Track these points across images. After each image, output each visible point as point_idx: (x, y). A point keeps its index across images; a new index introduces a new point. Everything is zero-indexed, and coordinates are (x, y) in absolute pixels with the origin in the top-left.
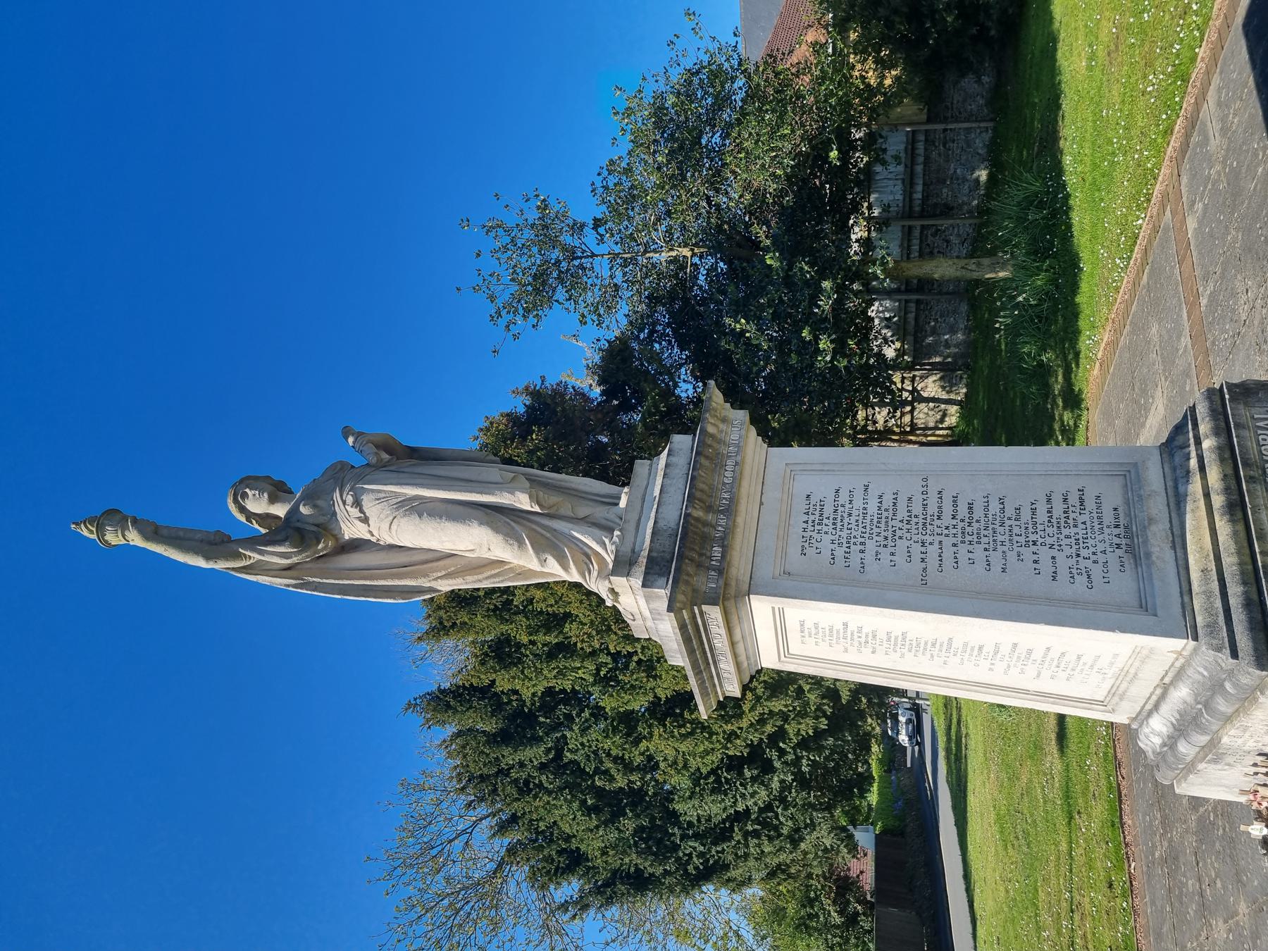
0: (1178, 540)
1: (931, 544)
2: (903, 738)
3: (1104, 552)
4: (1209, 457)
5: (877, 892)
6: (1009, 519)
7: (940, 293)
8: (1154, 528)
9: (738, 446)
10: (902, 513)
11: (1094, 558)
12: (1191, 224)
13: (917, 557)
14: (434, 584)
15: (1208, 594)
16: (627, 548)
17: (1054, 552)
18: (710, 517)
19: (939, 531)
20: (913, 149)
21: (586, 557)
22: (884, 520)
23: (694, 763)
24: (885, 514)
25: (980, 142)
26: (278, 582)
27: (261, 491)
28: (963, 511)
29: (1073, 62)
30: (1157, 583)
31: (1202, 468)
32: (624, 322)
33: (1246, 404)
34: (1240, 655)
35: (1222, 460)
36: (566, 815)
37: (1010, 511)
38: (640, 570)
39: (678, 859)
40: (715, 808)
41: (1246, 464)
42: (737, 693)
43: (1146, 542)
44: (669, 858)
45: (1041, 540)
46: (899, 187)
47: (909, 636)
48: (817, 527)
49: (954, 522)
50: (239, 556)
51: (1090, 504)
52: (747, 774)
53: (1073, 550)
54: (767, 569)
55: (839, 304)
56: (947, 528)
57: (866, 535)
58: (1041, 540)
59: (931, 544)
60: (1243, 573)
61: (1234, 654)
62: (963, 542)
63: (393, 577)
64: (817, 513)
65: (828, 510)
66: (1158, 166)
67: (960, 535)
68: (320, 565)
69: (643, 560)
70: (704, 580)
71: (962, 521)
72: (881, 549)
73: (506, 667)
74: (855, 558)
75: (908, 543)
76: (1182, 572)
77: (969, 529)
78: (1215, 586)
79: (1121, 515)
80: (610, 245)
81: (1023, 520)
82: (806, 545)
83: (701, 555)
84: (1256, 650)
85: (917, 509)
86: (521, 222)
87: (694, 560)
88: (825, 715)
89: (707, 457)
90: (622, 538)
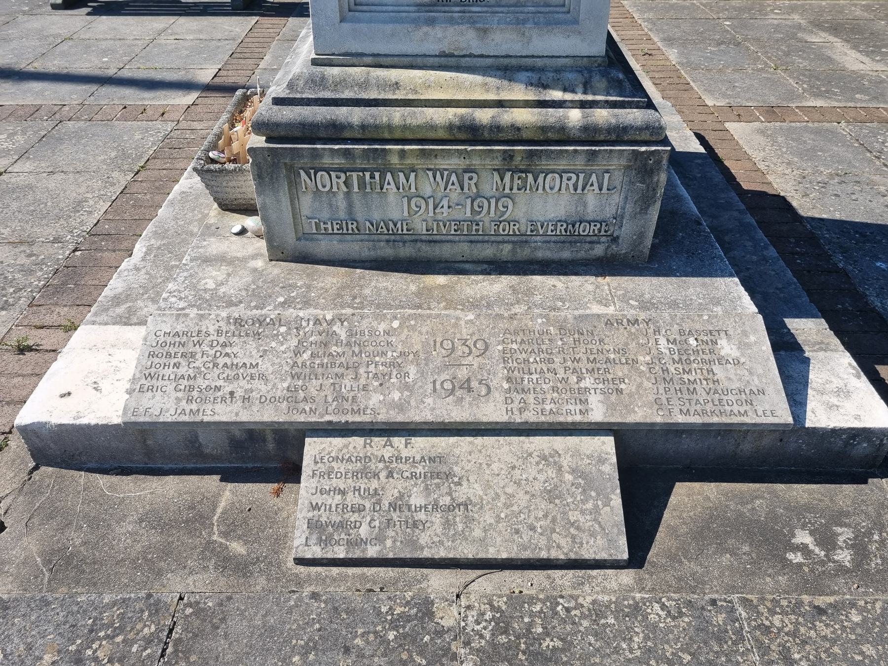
0: (452, 61)
4: (552, 115)
15: (365, 85)
30: (389, 28)
33: (628, 168)
34: (276, 107)
35: (544, 129)
41: (531, 154)
43: (452, 22)
60: (377, 127)
61: (278, 101)
76: (406, 60)
78: (373, 95)
84: (277, 125)
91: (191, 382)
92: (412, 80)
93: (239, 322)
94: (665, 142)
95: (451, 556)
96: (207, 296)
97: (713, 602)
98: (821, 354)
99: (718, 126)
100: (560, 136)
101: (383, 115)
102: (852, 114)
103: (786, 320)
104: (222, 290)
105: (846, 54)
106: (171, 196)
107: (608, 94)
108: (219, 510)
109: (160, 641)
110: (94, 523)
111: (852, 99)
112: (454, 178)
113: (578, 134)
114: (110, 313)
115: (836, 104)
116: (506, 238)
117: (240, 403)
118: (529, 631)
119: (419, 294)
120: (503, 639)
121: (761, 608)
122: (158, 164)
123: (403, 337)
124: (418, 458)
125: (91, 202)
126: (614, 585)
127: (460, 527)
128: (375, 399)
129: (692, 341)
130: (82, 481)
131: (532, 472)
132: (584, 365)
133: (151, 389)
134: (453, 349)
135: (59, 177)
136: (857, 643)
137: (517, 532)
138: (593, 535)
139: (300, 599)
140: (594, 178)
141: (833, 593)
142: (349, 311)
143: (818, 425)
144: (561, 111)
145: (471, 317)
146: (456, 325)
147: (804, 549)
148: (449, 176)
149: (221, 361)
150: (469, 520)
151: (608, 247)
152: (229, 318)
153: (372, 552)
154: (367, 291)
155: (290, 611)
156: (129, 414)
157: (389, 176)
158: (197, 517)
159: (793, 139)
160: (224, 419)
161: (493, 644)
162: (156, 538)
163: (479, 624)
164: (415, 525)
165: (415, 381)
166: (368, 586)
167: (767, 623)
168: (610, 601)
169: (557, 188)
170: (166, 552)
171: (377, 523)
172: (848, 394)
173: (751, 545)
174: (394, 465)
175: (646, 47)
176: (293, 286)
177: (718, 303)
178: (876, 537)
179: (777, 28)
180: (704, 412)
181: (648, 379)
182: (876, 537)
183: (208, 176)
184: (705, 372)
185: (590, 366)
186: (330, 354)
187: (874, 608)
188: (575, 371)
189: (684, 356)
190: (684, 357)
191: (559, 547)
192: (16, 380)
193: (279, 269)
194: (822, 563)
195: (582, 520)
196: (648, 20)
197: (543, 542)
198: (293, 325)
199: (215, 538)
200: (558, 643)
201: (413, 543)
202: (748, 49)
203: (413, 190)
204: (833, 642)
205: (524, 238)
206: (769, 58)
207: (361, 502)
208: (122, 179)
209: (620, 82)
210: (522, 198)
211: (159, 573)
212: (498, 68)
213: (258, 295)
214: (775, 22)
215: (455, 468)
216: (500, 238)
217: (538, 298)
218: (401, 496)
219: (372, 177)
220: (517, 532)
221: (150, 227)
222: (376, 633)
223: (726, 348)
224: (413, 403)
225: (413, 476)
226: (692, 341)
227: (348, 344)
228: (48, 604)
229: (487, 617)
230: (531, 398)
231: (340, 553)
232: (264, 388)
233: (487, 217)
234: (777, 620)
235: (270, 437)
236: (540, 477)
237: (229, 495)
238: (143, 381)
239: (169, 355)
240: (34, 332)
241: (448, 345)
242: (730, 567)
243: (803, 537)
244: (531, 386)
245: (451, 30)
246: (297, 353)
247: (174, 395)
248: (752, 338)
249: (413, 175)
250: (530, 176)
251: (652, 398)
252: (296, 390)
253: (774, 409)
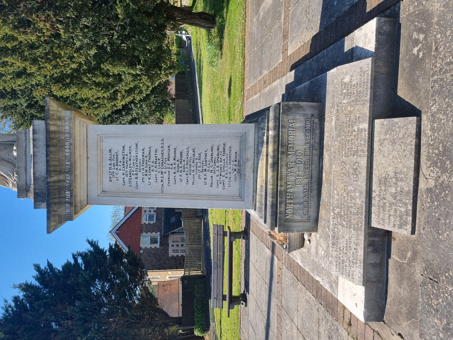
0: (255, 169)
1: (165, 173)
3: (230, 173)
4: (271, 140)
5: (176, 95)
6: (196, 159)
8: (248, 163)
9: (69, 133)
10: (153, 159)
11: (226, 176)
13: (159, 179)
15: (261, 196)
16: (23, 182)
17: (212, 174)
18: (61, 177)
19: (168, 166)
22: (145, 162)
24: (146, 159)
28: (178, 154)
30: (246, 187)
33: (287, 115)
35: (274, 142)
37: (197, 156)
38: (31, 196)
43: (245, 169)
45: (208, 169)
48: (116, 167)
49: (174, 162)
51: (227, 151)
53: (219, 173)
54: (95, 191)
56: (172, 165)
57: (138, 170)
58: (208, 169)
59: (165, 173)
61: (265, 222)
62: (178, 171)
64: (115, 159)
67: (177, 168)
70: (64, 208)
71: (178, 161)
72: (145, 177)
74: (134, 181)
75: (155, 173)
76: (255, 183)
77: (180, 165)
79: (238, 155)
81: (202, 159)
82: (111, 176)
83: (60, 198)
84: (272, 223)
85: (159, 156)
89: (53, 146)
90: (19, 177)
91: (351, 262)
93: (333, 244)
94: (279, 104)
95: (413, 180)
96: (326, 254)
97: (432, 87)
98: (355, 41)
99: (289, 58)
100: (277, 137)
101: (269, 191)
102: (287, 4)
103: (345, 51)
104: (325, 249)
105: (267, 2)
106: (302, 266)
107: (265, 122)
108: (398, 260)
109: (433, 283)
110: (400, 303)
111: (282, 3)
112: (289, 170)
113: (276, 132)
114: (335, 289)
115: (283, 10)
116: (311, 152)
117: (358, 247)
118: (437, 155)
119: (327, 183)
120: (439, 164)
121: (435, 70)
122: (295, 272)
123: (339, 190)
124: (379, 188)
125: (307, 297)
126: (426, 122)
127: (403, 176)
128: (358, 201)
129: (344, 91)
130: (388, 306)
131: (385, 149)
132: (350, 129)
133: (353, 275)
134: (344, 173)
135: (299, 308)
136: (446, 37)
137: (405, 156)
138: (407, 129)
139: (424, 234)
140: (290, 125)
141: (432, 42)
142: (331, 207)
143: (374, 47)
144: (269, 137)
145: (334, 166)
146: (337, 172)
147: (419, 51)
148: (288, 171)
149: (345, 251)
150: (401, 173)
151: (315, 117)
152: (332, 247)
153: (410, 207)
154: (326, 200)
155: (427, 238)
156: (360, 283)
157: (288, 190)
158: (400, 267)
159: (294, 30)
160: (363, 252)
161: (440, 168)
162: (405, 282)
163: (434, 172)
164: (402, 191)
165: (353, 187)
166: (422, 210)
167: (439, 69)
168: (430, 124)
169: (294, 137)
170: (409, 279)
171: (400, 205)
172: (366, 34)
173: (417, 70)
174: (381, 197)
175: (262, 82)
176: (324, 225)
177: (334, 81)
178: (416, 24)
179: (258, 29)
180: (367, 88)
181: (356, 107)
182: (416, 24)
183: (291, 249)
184: (354, 87)
185: (351, 127)
186: (344, 215)
187: (437, 29)
188: (352, 132)
189: (349, 94)
190: (349, 94)
191: (411, 141)
192: (359, 327)
193: (320, 229)
194: (423, 45)
195: (402, 133)
196: (254, 80)
197: (409, 147)
198: (335, 226)
199: (406, 262)
200: (441, 145)
201: (408, 193)
202: (264, 42)
203: (293, 183)
204: (445, 46)
205: (311, 146)
206: (267, 34)
207: (393, 209)
208: (300, 286)
209: (262, 119)
210: (297, 148)
211: (415, 282)
212: (258, 155)
213: (326, 237)
214: (256, 29)
215: (383, 176)
216: (311, 154)
217: (330, 143)
218: (392, 195)
219: (288, 196)
220: (405, 156)
221: (311, 274)
222: (435, 209)
223: (347, 80)
224: (360, 189)
225: (385, 191)
226: (344, 91)
227: (341, 208)
228: (421, 320)
229: (432, 169)
230: (360, 148)
231: (410, 218)
232: (354, 238)
233: (304, 159)
234: (438, 65)
235: (372, 239)
236: (387, 146)
237: (394, 256)
238: (350, 277)
239: (343, 268)
240: (345, 320)
241: (342, 175)
242: (423, 79)
243: (415, 50)
244: (356, 148)
245: (247, 169)
246: (343, 226)
247: (355, 268)
248: (344, 70)
249: (288, 183)
250: (289, 146)
251: (361, 106)
252: (355, 227)
253: (366, 64)
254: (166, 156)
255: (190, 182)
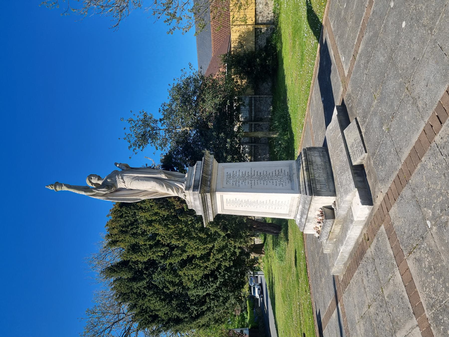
2: (257, 295)
4: (303, 161)
7: (261, 143)
10: (247, 175)
12: (312, 121)
14: (140, 198)
15: (303, 185)
16: (188, 185)
20: (251, 102)
21: (178, 189)
23: (195, 277)
25: (269, 101)
26: (101, 198)
27: (96, 177)
28: (259, 174)
29: (288, 82)
31: (302, 163)
32: (169, 149)
35: (305, 161)
36: (155, 304)
39: (189, 313)
40: (201, 293)
42: (213, 221)
44: (186, 312)
46: (248, 113)
47: (249, 201)
50: (92, 192)
51: (283, 172)
52: (210, 280)
54: (219, 187)
55: (232, 145)
61: (306, 194)
63: (130, 196)
65: (232, 175)
66: (306, 107)
68: (112, 194)
69: (192, 187)
73: (135, 253)
74: (237, 184)
80: (165, 127)
85: (250, 174)
86: (138, 119)
87: (204, 186)
88: (232, 260)
90: (187, 183)
92: (301, 179)
254: (253, 174)
255: (265, 184)
